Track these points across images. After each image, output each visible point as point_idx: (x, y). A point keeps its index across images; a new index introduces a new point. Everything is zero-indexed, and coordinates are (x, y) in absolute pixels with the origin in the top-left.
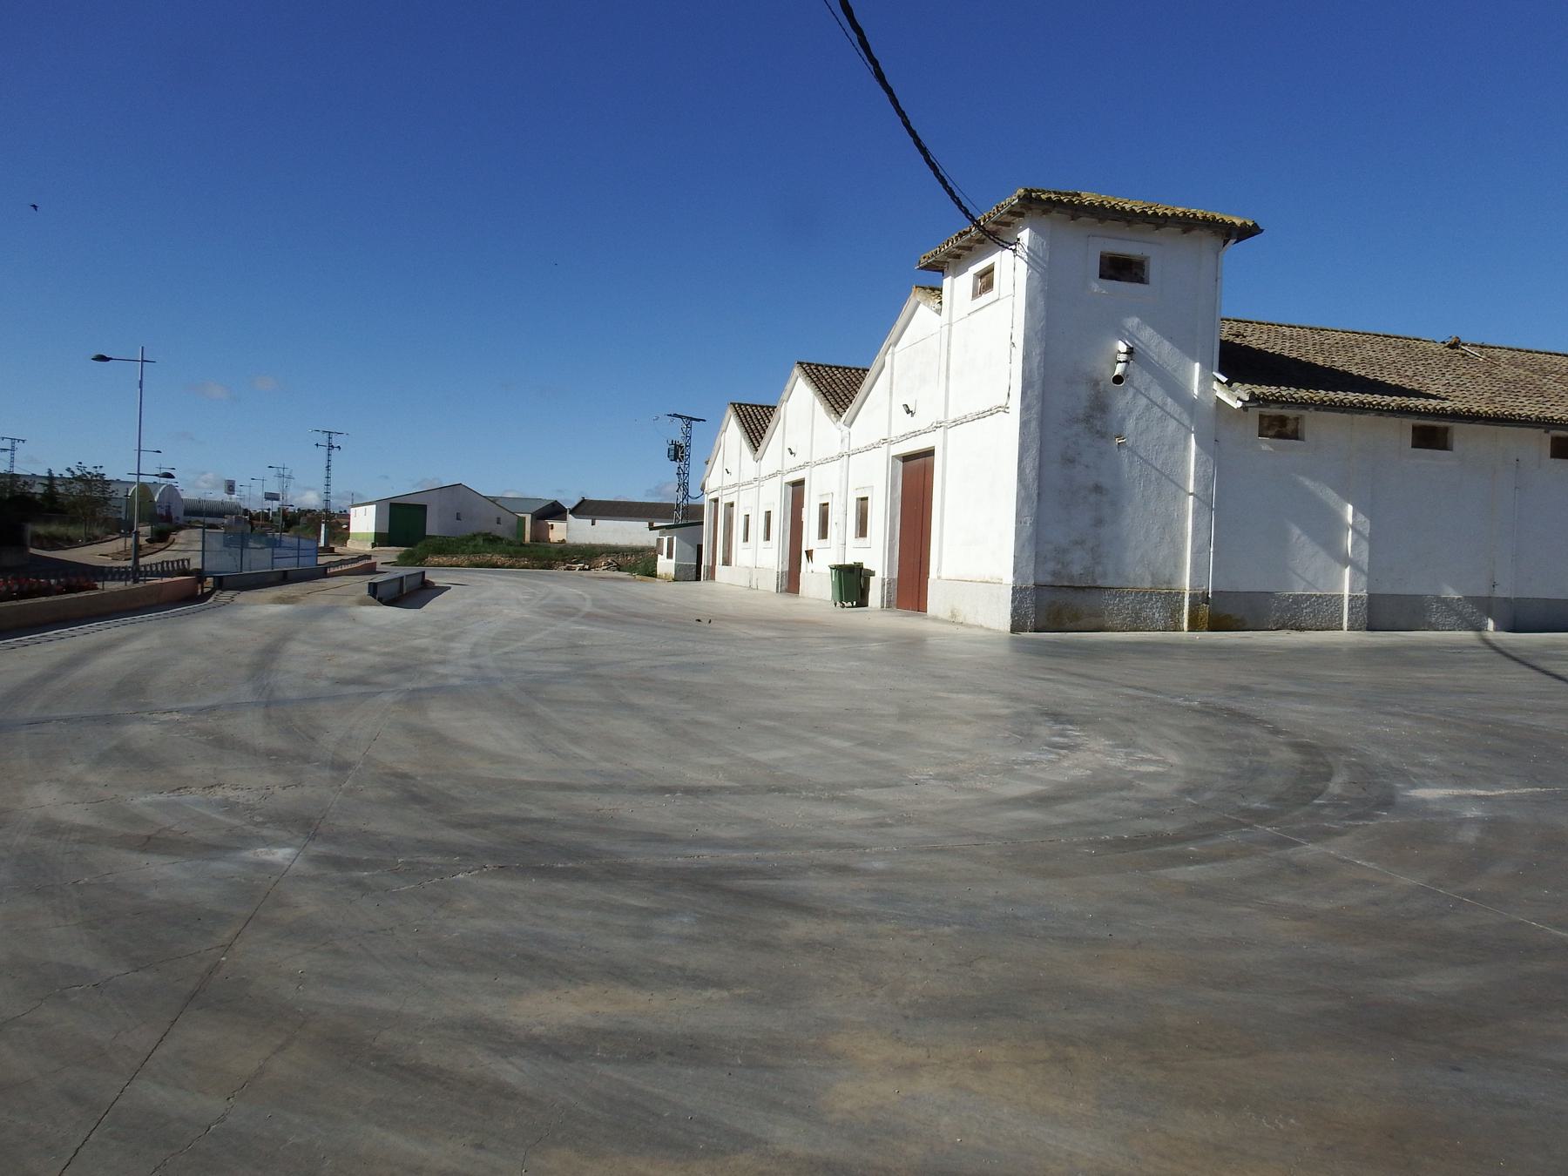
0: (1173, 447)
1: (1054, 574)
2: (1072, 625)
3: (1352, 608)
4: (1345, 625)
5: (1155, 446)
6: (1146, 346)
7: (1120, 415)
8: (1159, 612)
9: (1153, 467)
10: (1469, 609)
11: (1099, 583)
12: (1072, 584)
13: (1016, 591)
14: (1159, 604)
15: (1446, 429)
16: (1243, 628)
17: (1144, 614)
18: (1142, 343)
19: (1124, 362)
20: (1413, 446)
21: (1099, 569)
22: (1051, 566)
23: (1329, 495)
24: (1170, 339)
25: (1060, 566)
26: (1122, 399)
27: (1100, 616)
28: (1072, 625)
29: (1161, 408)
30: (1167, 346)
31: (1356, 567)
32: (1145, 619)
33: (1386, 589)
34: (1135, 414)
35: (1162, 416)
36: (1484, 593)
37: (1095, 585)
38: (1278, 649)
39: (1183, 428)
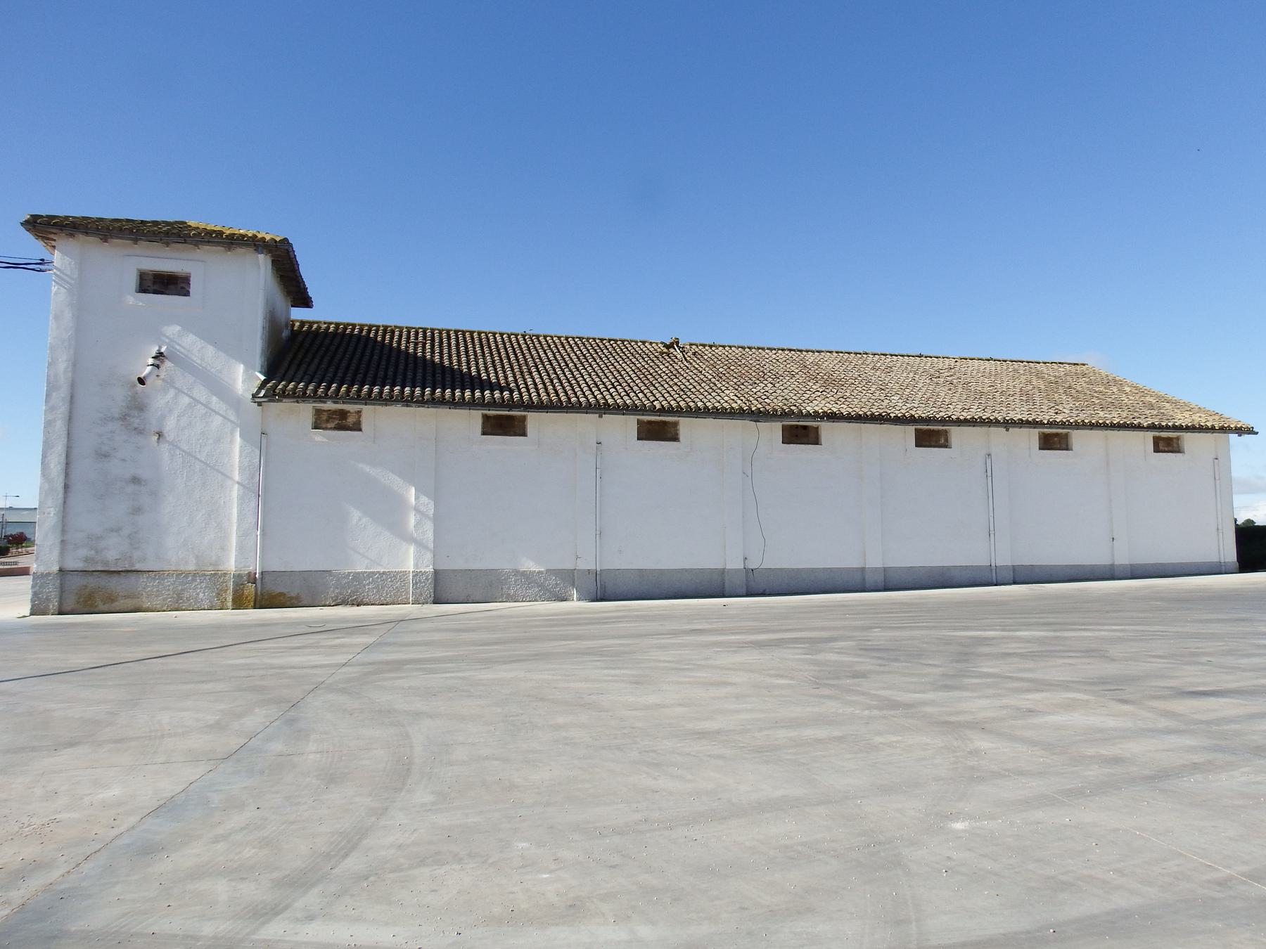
0: (218, 440)
1: (87, 560)
2: (105, 608)
3: (416, 583)
4: (575, 599)
5: (199, 440)
6: (189, 351)
7: (160, 413)
8: (204, 593)
9: (196, 458)
10: (552, 580)
11: (138, 567)
12: (107, 569)
13: (723, 571)
14: (204, 585)
15: (1067, 435)
16: (300, 604)
17: (186, 595)
18: (184, 348)
19: (151, 365)
20: (484, 433)
21: (137, 554)
22: (83, 552)
23: (393, 481)
24: (215, 344)
25: (93, 552)
26: (160, 400)
27: (138, 598)
28: (105, 608)
29: (206, 406)
30: (210, 350)
31: (420, 544)
32: (188, 599)
33: (457, 563)
34: (176, 413)
35: (206, 413)
36: (568, 565)
37: (133, 569)
38: (527, 617)
39: (229, 423)
